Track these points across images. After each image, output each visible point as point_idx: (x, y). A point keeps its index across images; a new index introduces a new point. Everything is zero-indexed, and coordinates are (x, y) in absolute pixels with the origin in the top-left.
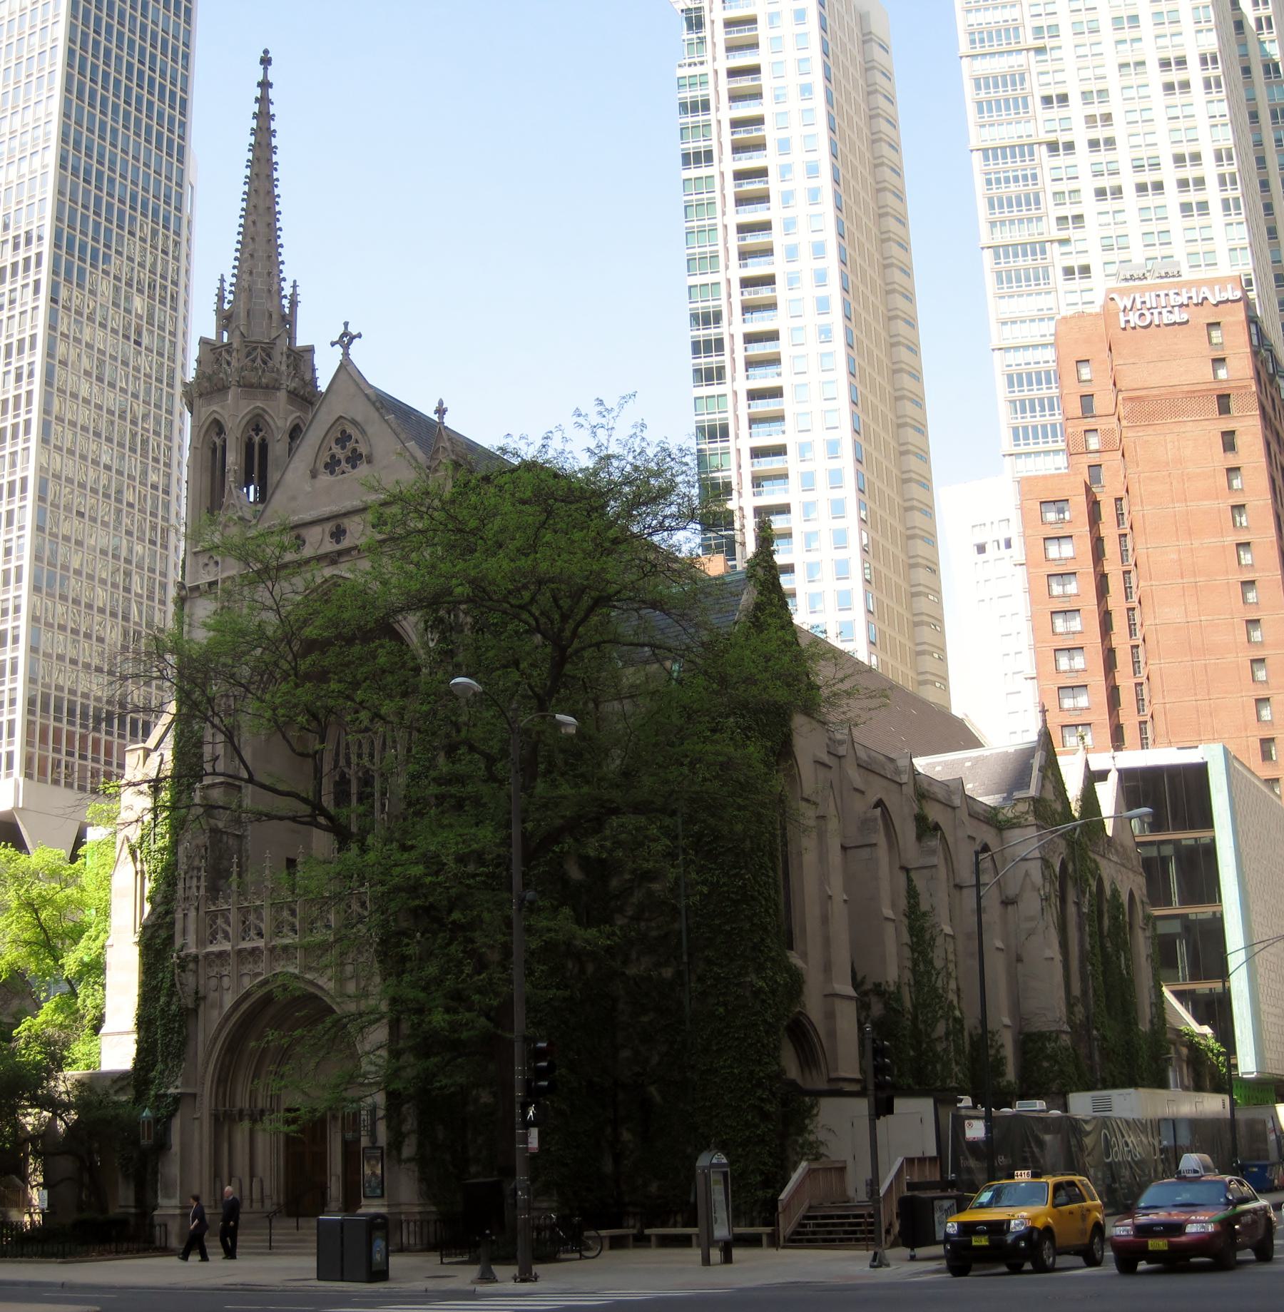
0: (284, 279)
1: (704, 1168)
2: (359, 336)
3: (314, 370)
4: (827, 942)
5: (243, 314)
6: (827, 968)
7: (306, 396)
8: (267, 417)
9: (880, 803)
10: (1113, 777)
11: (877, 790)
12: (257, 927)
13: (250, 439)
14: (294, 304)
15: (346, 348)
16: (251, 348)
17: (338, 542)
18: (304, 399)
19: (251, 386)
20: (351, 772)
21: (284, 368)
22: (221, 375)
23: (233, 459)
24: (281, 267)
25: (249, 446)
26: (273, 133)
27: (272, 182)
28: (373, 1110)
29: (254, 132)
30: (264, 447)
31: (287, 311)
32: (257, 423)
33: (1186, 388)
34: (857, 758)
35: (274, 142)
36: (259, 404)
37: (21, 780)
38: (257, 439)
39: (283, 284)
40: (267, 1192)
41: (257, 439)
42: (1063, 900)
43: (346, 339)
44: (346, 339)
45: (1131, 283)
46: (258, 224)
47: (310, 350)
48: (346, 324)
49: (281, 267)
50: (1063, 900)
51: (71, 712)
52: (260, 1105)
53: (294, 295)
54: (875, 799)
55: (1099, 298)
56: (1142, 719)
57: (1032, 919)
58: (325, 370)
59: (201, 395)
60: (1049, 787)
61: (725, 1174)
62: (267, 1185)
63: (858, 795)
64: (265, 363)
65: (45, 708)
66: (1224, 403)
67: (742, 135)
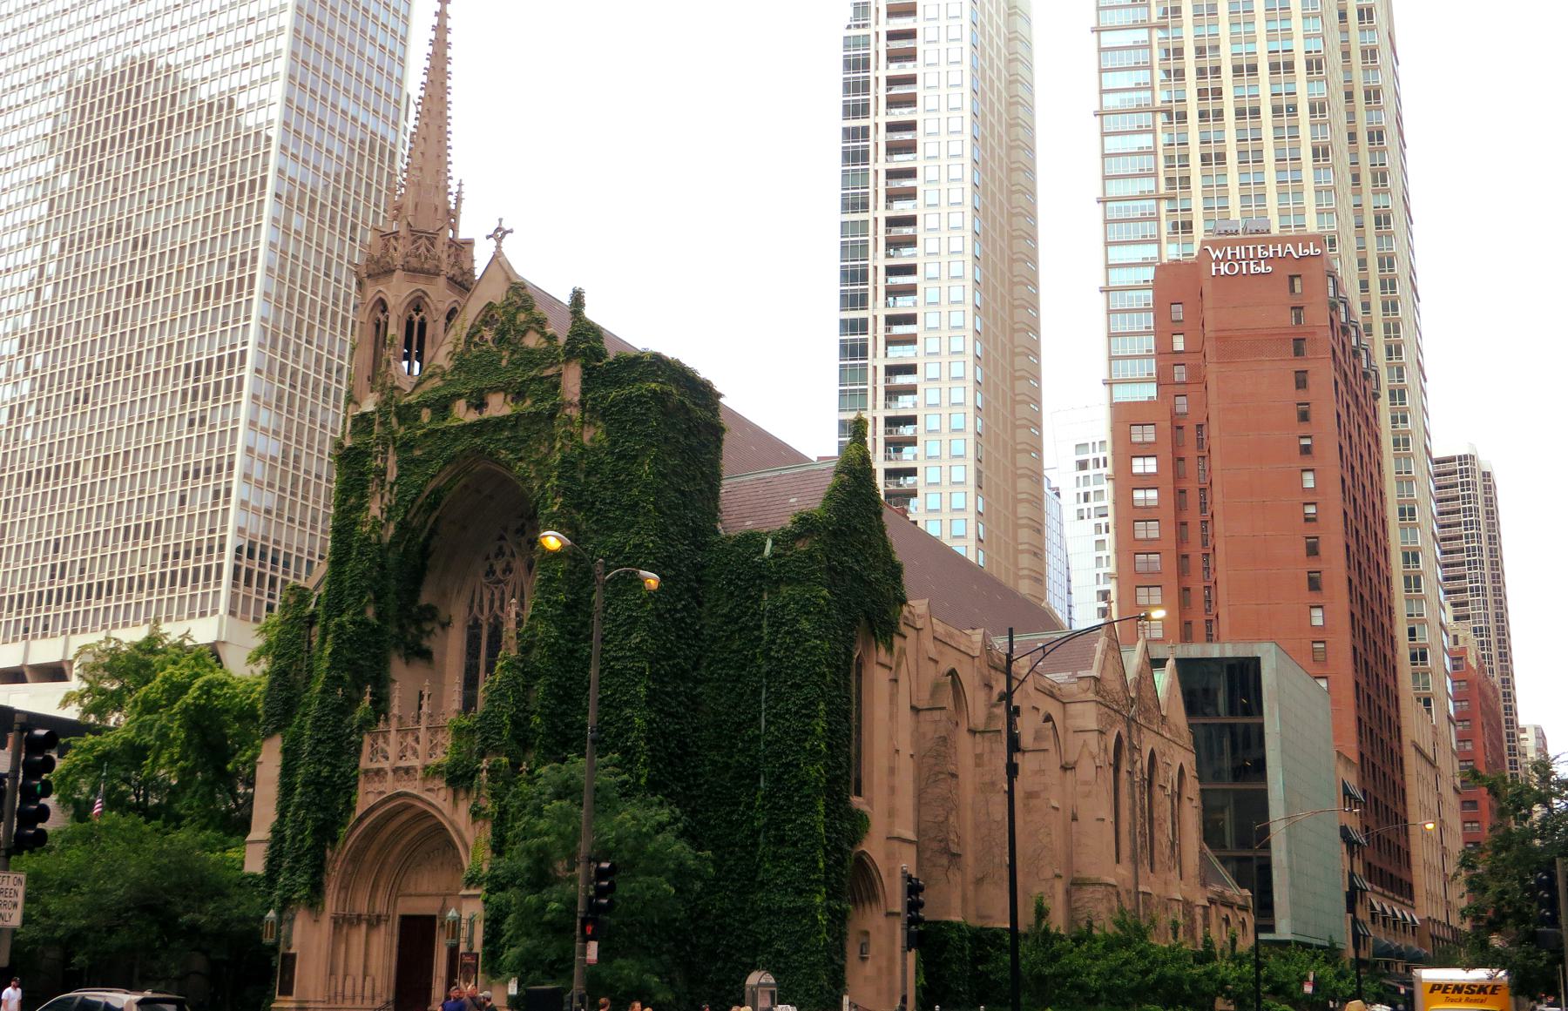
0: (451, 178)
1: (752, 987)
2: (511, 231)
3: (473, 261)
4: (892, 790)
5: (411, 206)
6: (891, 813)
7: (462, 283)
8: (427, 299)
9: (953, 673)
10: (1170, 663)
11: (949, 661)
12: (383, 751)
13: (411, 317)
14: (459, 200)
15: (499, 240)
16: (416, 235)
17: (480, 413)
18: (460, 284)
19: (415, 271)
20: (483, 618)
21: (444, 256)
22: (388, 259)
23: (395, 330)
24: (449, 167)
25: (410, 324)
26: (448, 45)
27: (445, 90)
28: (471, 922)
29: (432, 43)
30: (422, 325)
31: (453, 207)
32: (417, 304)
33: (1265, 332)
34: (934, 631)
35: (449, 53)
36: (421, 287)
37: (225, 617)
38: (417, 319)
39: (450, 182)
40: (378, 990)
41: (417, 319)
42: (1117, 770)
43: (500, 234)
44: (500, 234)
45: (1224, 237)
46: (431, 126)
47: (470, 243)
48: (500, 220)
49: (449, 167)
50: (1117, 770)
51: (263, 555)
52: (377, 912)
53: (459, 193)
54: (949, 668)
55: (1196, 249)
56: (1209, 618)
57: (1086, 783)
58: (481, 258)
59: (369, 276)
60: (1109, 668)
61: (772, 993)
62: (378, 984)
63: (932, 663)
64: (428, 251)
65: (251, 555)
66: (1299, 346)
67: (898, 90)
